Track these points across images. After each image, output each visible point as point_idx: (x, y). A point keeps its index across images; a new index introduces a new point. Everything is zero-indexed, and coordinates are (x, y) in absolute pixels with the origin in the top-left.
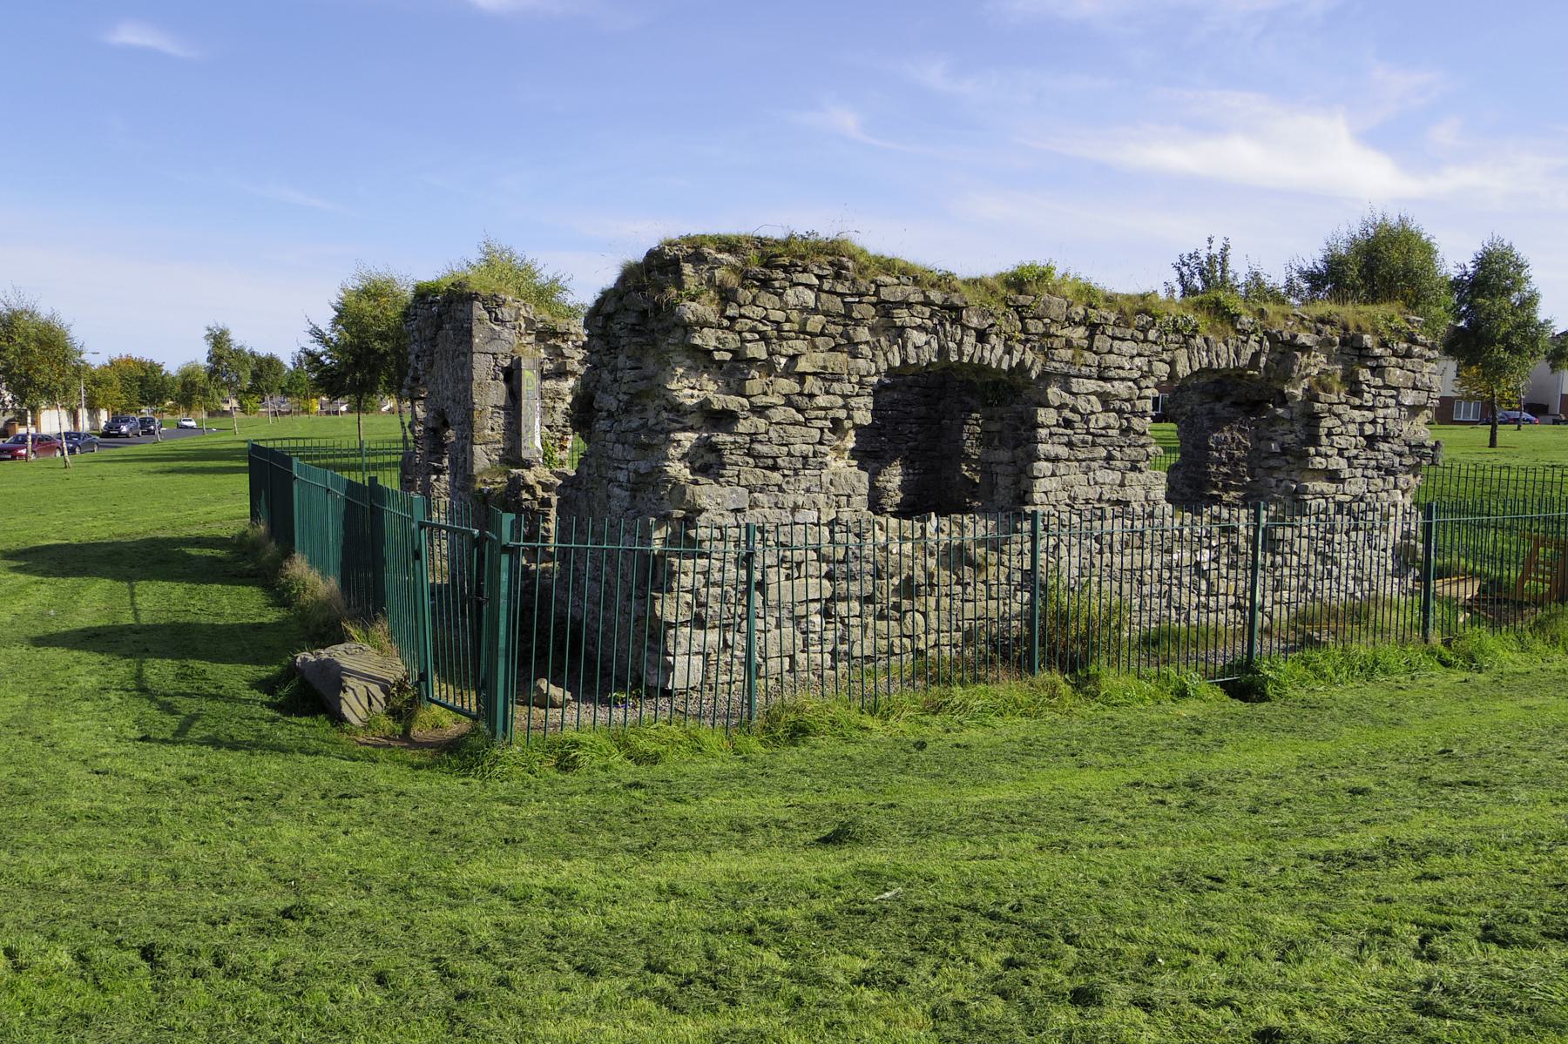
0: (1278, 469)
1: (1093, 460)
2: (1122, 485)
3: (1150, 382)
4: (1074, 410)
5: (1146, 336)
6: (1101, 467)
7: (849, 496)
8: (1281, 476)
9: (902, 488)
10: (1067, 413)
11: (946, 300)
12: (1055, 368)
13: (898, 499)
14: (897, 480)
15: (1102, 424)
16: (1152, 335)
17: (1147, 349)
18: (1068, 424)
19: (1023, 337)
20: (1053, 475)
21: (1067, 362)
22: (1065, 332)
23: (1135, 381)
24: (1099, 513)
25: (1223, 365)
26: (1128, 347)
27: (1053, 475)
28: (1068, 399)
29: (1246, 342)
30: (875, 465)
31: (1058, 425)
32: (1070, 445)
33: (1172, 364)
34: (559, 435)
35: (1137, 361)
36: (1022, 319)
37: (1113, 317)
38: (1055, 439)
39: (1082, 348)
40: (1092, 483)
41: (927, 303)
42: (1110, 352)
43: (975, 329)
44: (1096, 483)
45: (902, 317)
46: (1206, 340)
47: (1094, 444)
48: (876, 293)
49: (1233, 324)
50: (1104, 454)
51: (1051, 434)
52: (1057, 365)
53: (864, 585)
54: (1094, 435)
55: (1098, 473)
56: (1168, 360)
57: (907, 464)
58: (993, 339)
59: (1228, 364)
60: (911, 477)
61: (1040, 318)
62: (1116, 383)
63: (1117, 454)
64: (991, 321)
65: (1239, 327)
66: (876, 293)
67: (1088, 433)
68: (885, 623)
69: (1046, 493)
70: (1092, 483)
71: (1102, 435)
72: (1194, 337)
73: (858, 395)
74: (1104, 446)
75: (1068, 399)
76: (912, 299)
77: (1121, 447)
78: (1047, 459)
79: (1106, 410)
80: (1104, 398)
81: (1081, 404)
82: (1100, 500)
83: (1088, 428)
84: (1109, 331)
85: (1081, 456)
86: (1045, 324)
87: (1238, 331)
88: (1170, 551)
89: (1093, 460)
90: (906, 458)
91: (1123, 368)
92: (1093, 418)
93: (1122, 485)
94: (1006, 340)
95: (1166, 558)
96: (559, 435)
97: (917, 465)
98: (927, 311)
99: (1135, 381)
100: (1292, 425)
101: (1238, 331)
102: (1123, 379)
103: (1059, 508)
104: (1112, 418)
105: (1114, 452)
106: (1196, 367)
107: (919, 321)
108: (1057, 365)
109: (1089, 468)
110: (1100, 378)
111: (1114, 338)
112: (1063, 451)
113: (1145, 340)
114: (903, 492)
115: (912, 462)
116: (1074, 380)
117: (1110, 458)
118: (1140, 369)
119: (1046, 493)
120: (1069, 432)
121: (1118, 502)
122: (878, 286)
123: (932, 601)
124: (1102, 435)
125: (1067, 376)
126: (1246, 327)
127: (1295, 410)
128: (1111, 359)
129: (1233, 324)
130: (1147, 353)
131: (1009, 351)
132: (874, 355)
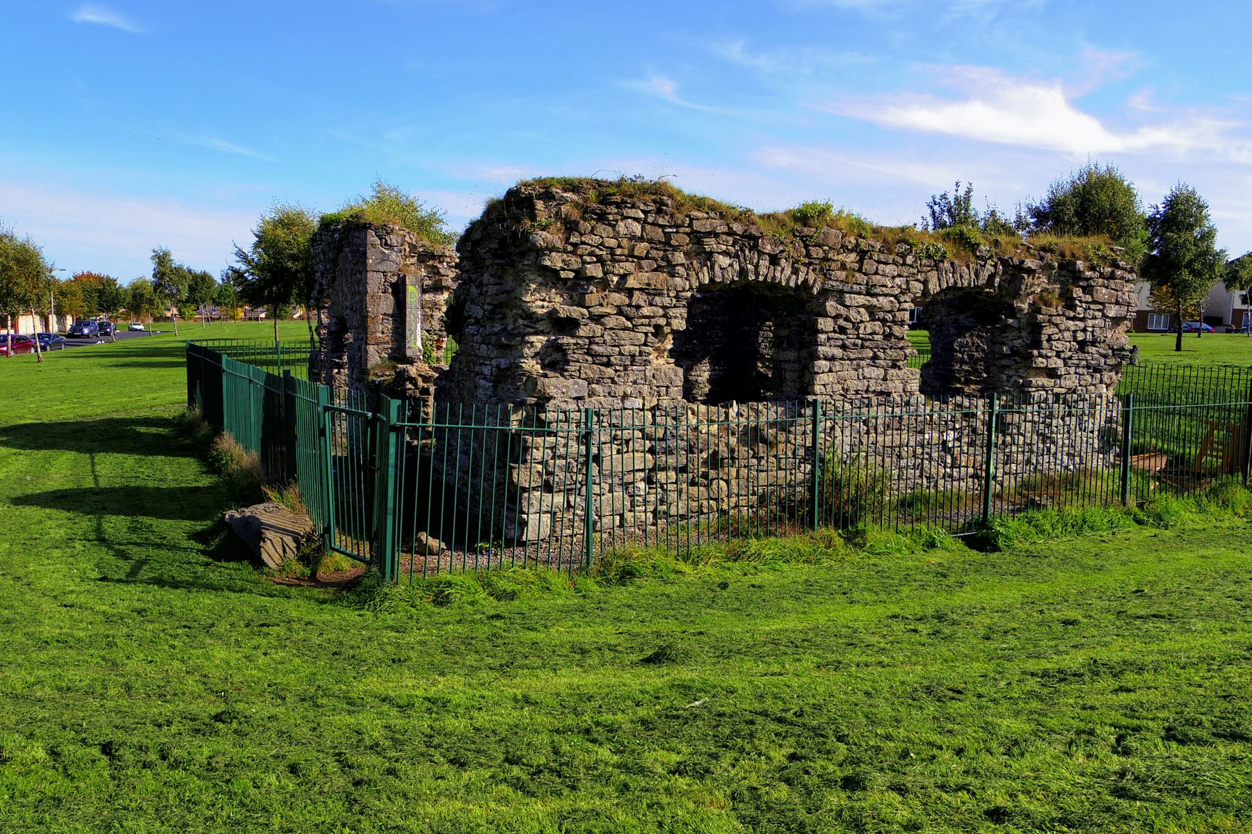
0: (1008, 367)
2: (885, 379)
4: (847, 319)
5: (904, 261)
8: (1011, 373)
10: (841, 322)
11: (746, 231)
13: (706, 390)
14: (706, 375)
16: (910, 260)
17: (905, 271)
18: (842, 330)
20: (831, 371)
21: (842, 281)
22: (840, 257)
24: (866, 401)
27: (831, 371)
28: (842, 310)
29: (984, 266)
31: (834, 331)
32: (844, 347)
33: (925, 283)
35: (898, 280)
38: (832, 342)
40: (861, 377)
41: (731, 233)
42: (876, 273)
43: (769, 254)
47: (863, 347)
48: (690, 225)
49: (974, 251)
50: (871, 354)
51: (829, 339)
52: (834, 284)
55: (866, 370)
59: (969, 284)
61: (820, 246)
62: (881, 298)
63: (881, 355)
64: (781, 248)
66: (690, 225)
67: (858, 338)
69: (824, 385)
71: (870, 340)
72: (943, 262)
74: (871, 348)
75: (842, 310)
78: (826, 359)
79: (873, 319)
80: (871, 310)
81: (853, 314)
82: (867, 391)
83: (858, 334)
85: (852, 356)
87: (978, 257)
88: (922, 432)
89: (862, 359)
91: (886, 286)
92: (862, 326)
94: (793, 263)
95: (919, 437)
99: (896, 297)
101: (978, 257)
102: (886, 295)
105: (879, 353)
106: (944, 286)
107: (724, 248)
108: (834, 284)
109: (858, 365)
111: (879, 262)
112: (838, 352)
113: (904, 264)
116: (847, 295)
117: (875, 357)
118: (900, 287)
119: (824, 385)
121: (881, 393)
123: (733, 472)
124: (870, 340)
129: (974, 251)
131: (795, 272)
132: (688, 274)
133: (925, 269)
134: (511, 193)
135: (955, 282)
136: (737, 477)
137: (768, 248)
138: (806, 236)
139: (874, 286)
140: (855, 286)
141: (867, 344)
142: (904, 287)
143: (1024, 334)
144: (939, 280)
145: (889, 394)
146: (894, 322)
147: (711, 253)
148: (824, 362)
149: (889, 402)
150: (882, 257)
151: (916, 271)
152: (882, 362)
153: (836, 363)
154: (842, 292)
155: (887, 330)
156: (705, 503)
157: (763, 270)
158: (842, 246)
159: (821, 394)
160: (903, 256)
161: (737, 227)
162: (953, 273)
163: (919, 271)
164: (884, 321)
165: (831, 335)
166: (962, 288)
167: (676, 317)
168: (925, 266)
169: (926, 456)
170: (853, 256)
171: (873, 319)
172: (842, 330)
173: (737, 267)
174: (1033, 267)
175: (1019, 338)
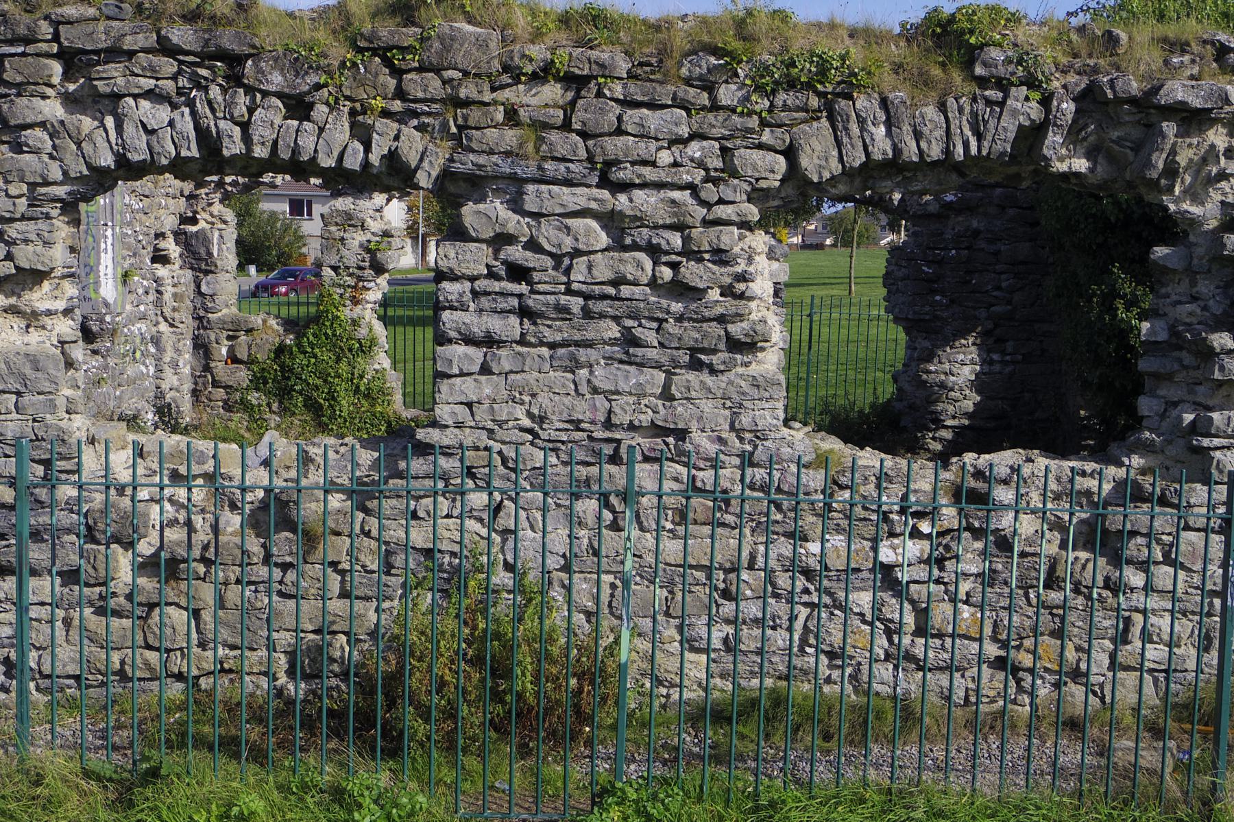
0: (1169, 377)
1: (589, 344)
2: (667, 395)
3: (736, 190)
4: (533, 245)
5: (713, 99)
6: (609, 359)
7: (19, 394)
9: (979, 384)
10: (515, 253)
12: (480, 167)
13: (969, 405)
14: (967, 373)
15: (607, 275)
16: (727, 94)
17: (716, 124)
18: (518, 273)
19: (397, 106)
20: (485, 370)
21: (508, 154)
22: (506, 94)
23: (692, 188)
25: (935, 152)
27: (485, 370)
29: (1002, 104)
30: (927, 344)
31: (492, 275)
32: (525, 312)
33: (790, 153)
38: (485, 302)
39: (546, 126)
40: (584, 389)
41: (166, 48)
42: (620, 132)
43: (279, 95)
44: (595, 391)
45: (114, 76)
46: (884, 103)
47: (587, 314)
48: (56, 38)
49: (968, 65)
50: (614, 332)
51: (475, 294)
52: (482, 160)
53: (60, 552)
54: (587, 297)
55: (598, 371)
57: (985, 349)
58: (320, 111)
59: (948, 152)
60: (997, 367)
62: (639, 194)
64: (313, 79)
65: (979, 70)
66: (56, 38)
67: (569, 292)
69: (469, 405)
71: (604, 297)
73: (23, 218)
74: (616, 319)
75: (513, 222)
76: (128, 43)
78: (469, 340)
80: (611, 220)
81: (548, 235)
82: (608, 424)
84: (618, 90)
85: (550, 336)
87: (982, 82)
89: (589, 344)
90: (985, 334)
91: (653, 164)
92: (581, 263)
93: (667, 395)
94: (353, 113)
96: (350, 281)
97: (1010, 346)
99: (692, 188)
100: (1193, 283)
104: (640, 265)
105: (638, 332)
107: (148, 83)
108: (482, 160)
109: (573, 358)
113: (715, 107)
114: (978, 392)
115: (1000, 341)
116: (531, 188)
117: (630, 340)
118: (701, 164)
119: (469, 405)
120: (524, 288)
121: (657, 430)
123: (207, 593)
124: (604, 297)
125: (518, 182)
126: (1002, 71)
127: (1200, 251)
128: (614, 146)
129: (968, 65)
130: (717, 132)
131: (363, 135)
137: (276, 80)
139: (616, 163)
140: (549, 166)
142: (716, 163)
143: (1205, 287)
145: (681, 434)
147: (117, 97)
148: (461, 349)
152: (652, 354)
153: (503, 353)
154: (518, 182)
157: (262, 132)
161: (180, 35)
162: (889, 124)
164: (654, 251)
165: (481, 284)
166: (924, 165)
167: (26, 241)
168: (785, 107)
172: (518, 273)
173: (186, 125)
174: (1197, 103)
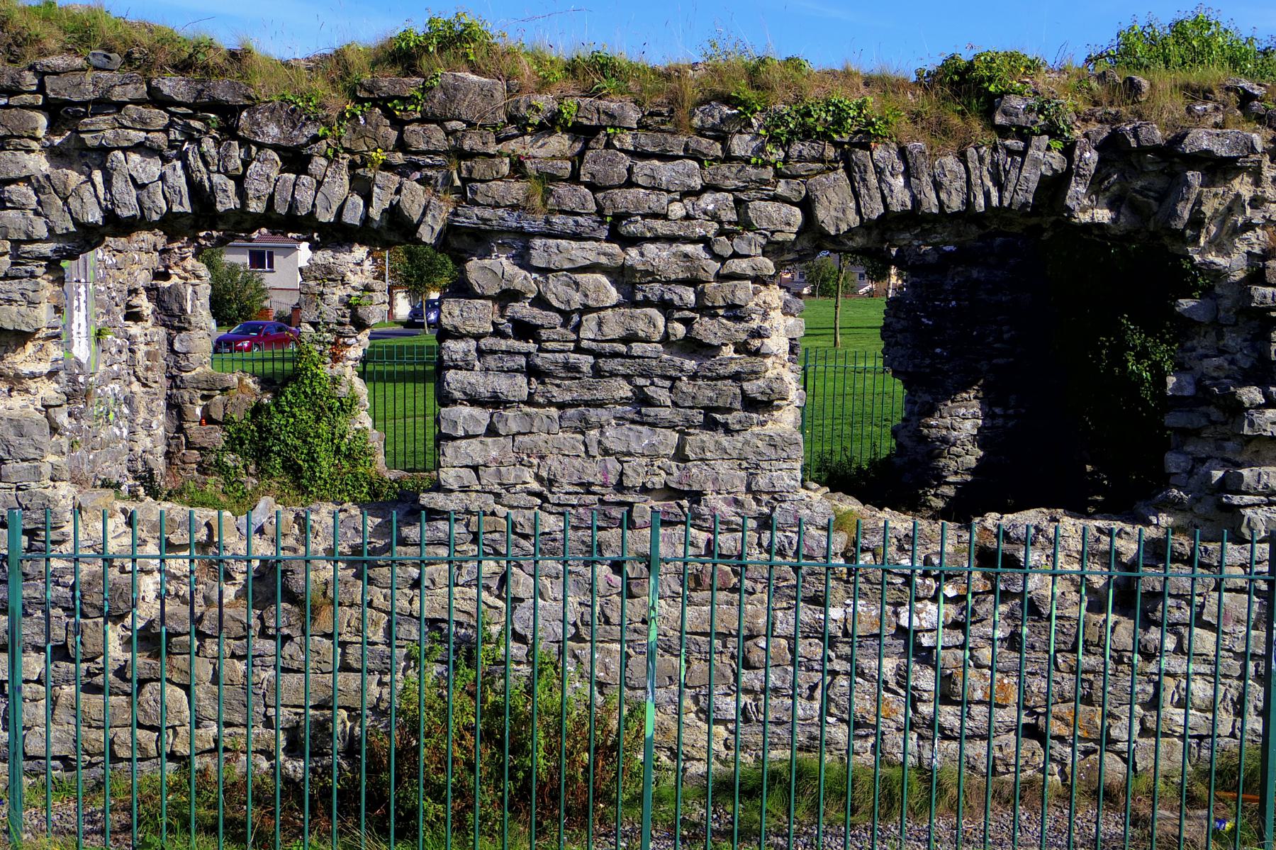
0: (1196, 433)
2: (680, 456)
4: (540, 302)
5: (726, 149)
8: (1203, 449)
9: (982, 438)
10: (522, 310)
11: (200, 92)
13: (971, 461)
14: (969, 427)
15: (618, 332)
16: (741, 145)
17: (730, 176)
18: (525, 330)
19: (399, 158)
20: (492, 431)
21: (514, 207)
22: (513, 145)
23: (705, 241)
24: (616, 513)
26: (687, 173)
27: (492, 431)
28: (521, 279)
29: (1023, 154)
30: (927, 398)
31: (498, 333)
32: (532, 372)
33: (807, 205)
34: (330, 337)
35: (708, 201)
36: (398, 124)
37: (633, 116)
38: (491, 361)
39: (553, 178)
40: (594, 450)
41: (157, 99)
42: (630, 184)
43: (275, 148)
44: (606, 452)
45: (101, 129)
47: (597, 372)
48: (41, 89)
49: (987, 114)
50: (625, 390)
51: (481, 353)
52: (487, 213)
54: (597, 355)
55: (610, 432)
56: (795, 197)
57: (987, 402)
58: (318, 164)
59: (968, 203)
60: (999, 422)
61: (440, 121)
62: (650, 249)
63: (661, 393)
64: (310, 130)
65: (999, 119)
66: (41, 89)
67: (579, 350)
68: (97, 699)
69: (475, 468)
70: (594, 450)
72: (866, 147)
74: (628, 378)
75: (521, 279)
76: (117, 94)
77: (674, 379)
78: (474, 401)
79: (629, 301)
80: (622, 276)
82: (620, 487)
83: (577, 341)
85: (559, 395)
86: (448, 133)
87: (1003, 131)
88: (819, 601)
91: (665, 217)
92: (590, 320)
94: (352, 166)
95: (808, 614)
96: (330, 337)
98: (159, 118)
99: (705, 241)
100: (1220, 336)
101: (1003, 131)
102: (671, 239)
103: (507, 498)
105: (651, 391)
106: (876, 210)
108: (487, 213)
110: (614, 237)
111: (639, 154)
112: (519, 386)
113: (728, 158)
116: (538, 242)
117: (642, 400)
118: (714, 217)
119: (475, 468)
120: (531, 346)
121: (671, 493)
122: (41, 75)
123: (203, 669)
125: (525, 236)
126: (1022, 120)
131: (363, 188)
132: (39, 202)
133: (800, 168)
134: (595, 56)
135: (916, 202)
136: (216, 680)
137: (272, 132)
138: (391, 99)
139: (627, 215)
140: (557, 219)
141: (608, 365)
144: (856, 195)
146: (703, 309)
147: (104, 151)
148: (466, 410)
149: (698, 516)
150: (647, 142)
151: (768, 173)
152: (665, 413)
153: (509, 413)
154: (525, 236)
155: (679, 330)
156: (124, 734)
157: (256, 186)
158: (512, 119)
159: (465, 489)
160: (722, 137)
161: (171, 85)
162: (907, 174)
163: (779, 175)
164: (666, 307)
165: (486, 343)
166: (943, 215)
168: (801, 158)
169: (839, 666)
170: (559, 143)
171: (629, 301)
172: (525, 330)
175: (1221, 352)
